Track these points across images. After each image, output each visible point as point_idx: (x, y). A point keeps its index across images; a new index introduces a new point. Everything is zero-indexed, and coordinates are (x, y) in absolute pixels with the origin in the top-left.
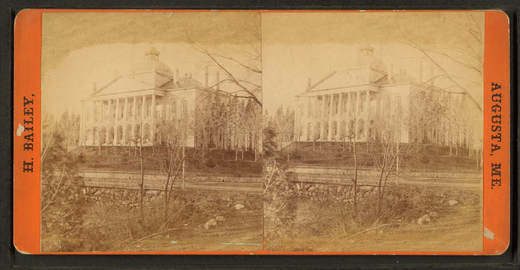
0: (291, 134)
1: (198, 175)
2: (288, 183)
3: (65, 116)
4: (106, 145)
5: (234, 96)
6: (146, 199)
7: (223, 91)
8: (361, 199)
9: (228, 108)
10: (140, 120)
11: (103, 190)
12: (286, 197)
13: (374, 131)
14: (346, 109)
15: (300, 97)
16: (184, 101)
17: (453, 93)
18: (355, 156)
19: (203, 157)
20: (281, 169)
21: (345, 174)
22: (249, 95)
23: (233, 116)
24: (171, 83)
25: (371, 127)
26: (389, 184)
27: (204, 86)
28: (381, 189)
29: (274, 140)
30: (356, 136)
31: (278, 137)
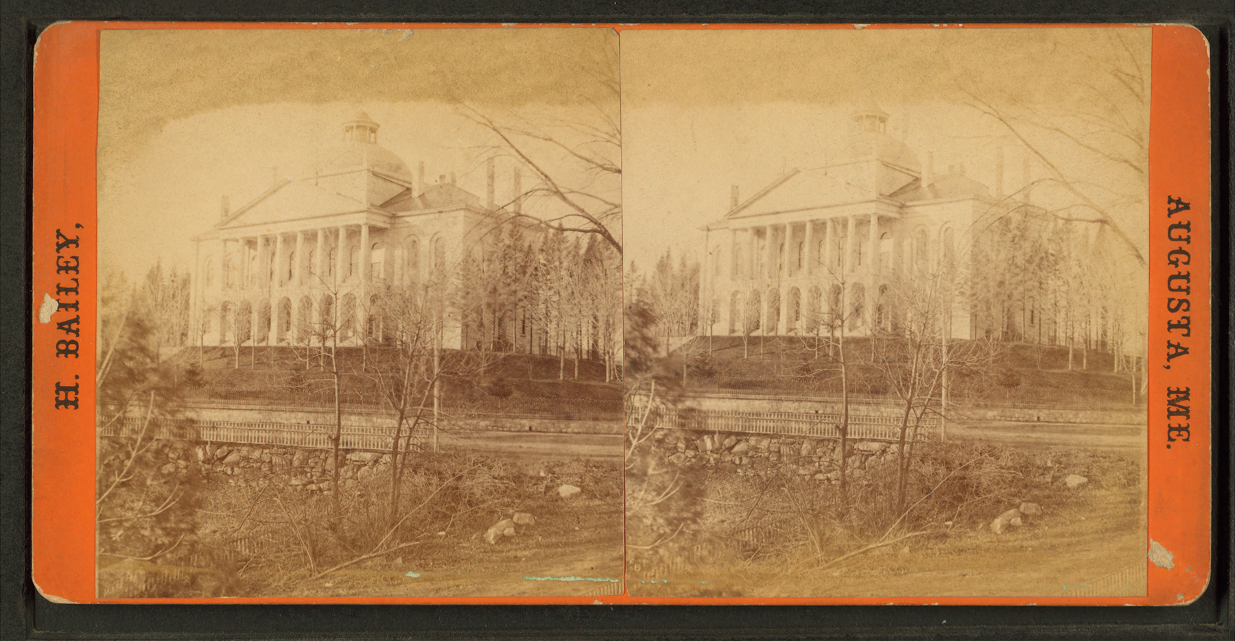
0: (691, 319)
1: (471, 417)
4: (252, 345)
5: (557, 229)
6: (346, 472)
7: (529, 217)
8: (857, 473)
10: (333, 286)
12: (680, 469)
13: (888, 312)
14: (821, 259)
16: (436, 240)
17: (1077, 220)
18: (843, 370)
19: (482, 374)
20: (668, 400)
21: (820, 412)
22: (591, 226)
23: (552, 276)
24: (406, 197)
25: (882, 301)
26: (925, 436)
28: (905, 448)
29: (651, 332)
30: (846, 323)
31: (661, 326)
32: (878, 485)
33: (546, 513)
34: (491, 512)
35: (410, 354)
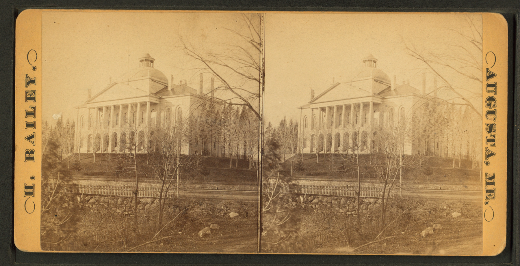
1: (192, 183)
2: (291, 195)
3: (59, 123)
4: (101, 152)
5: (229, 104)
6: (140, 207)
7: (217, 98)
8: (364, 211)
9: (222, 115)
11: (97, 198)
12: (290, 210)
13: (377, 143)
15: (303, 109)
16: (179, 108)
17: (457, 104)
18: (358, 168)
19: (197, 165)
20: (285, 181)
21: (348, 186)
22: (243, 102)
23: (227, 123)
24: (166, 90)
25: (375, 139)
26: (393, 196)
27: (198, 93)
28: (384, 201)
29: (277, 152)
30: (360, 148)
31: (282, 149)
32: (373, 217)
33: (224, 224)
34: (201, 224)
35: (167, 156)
